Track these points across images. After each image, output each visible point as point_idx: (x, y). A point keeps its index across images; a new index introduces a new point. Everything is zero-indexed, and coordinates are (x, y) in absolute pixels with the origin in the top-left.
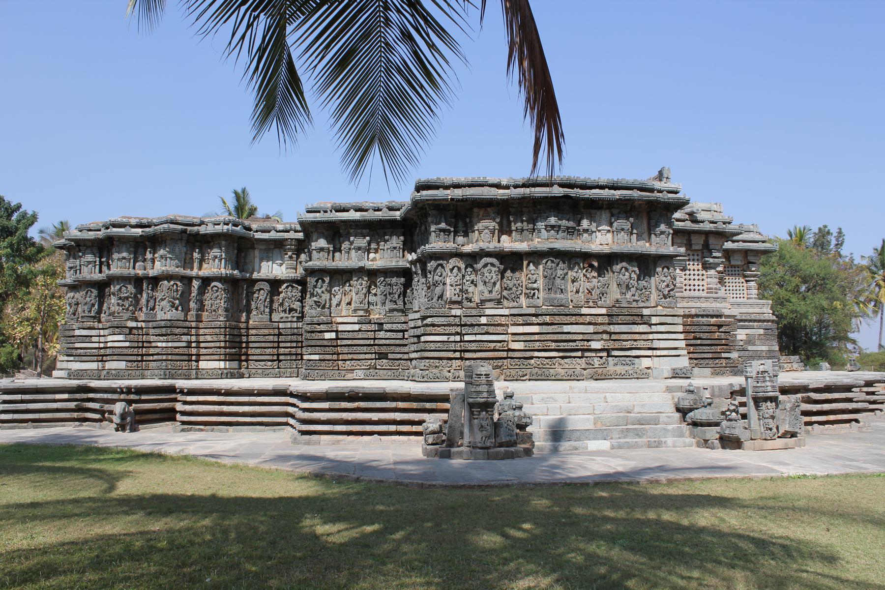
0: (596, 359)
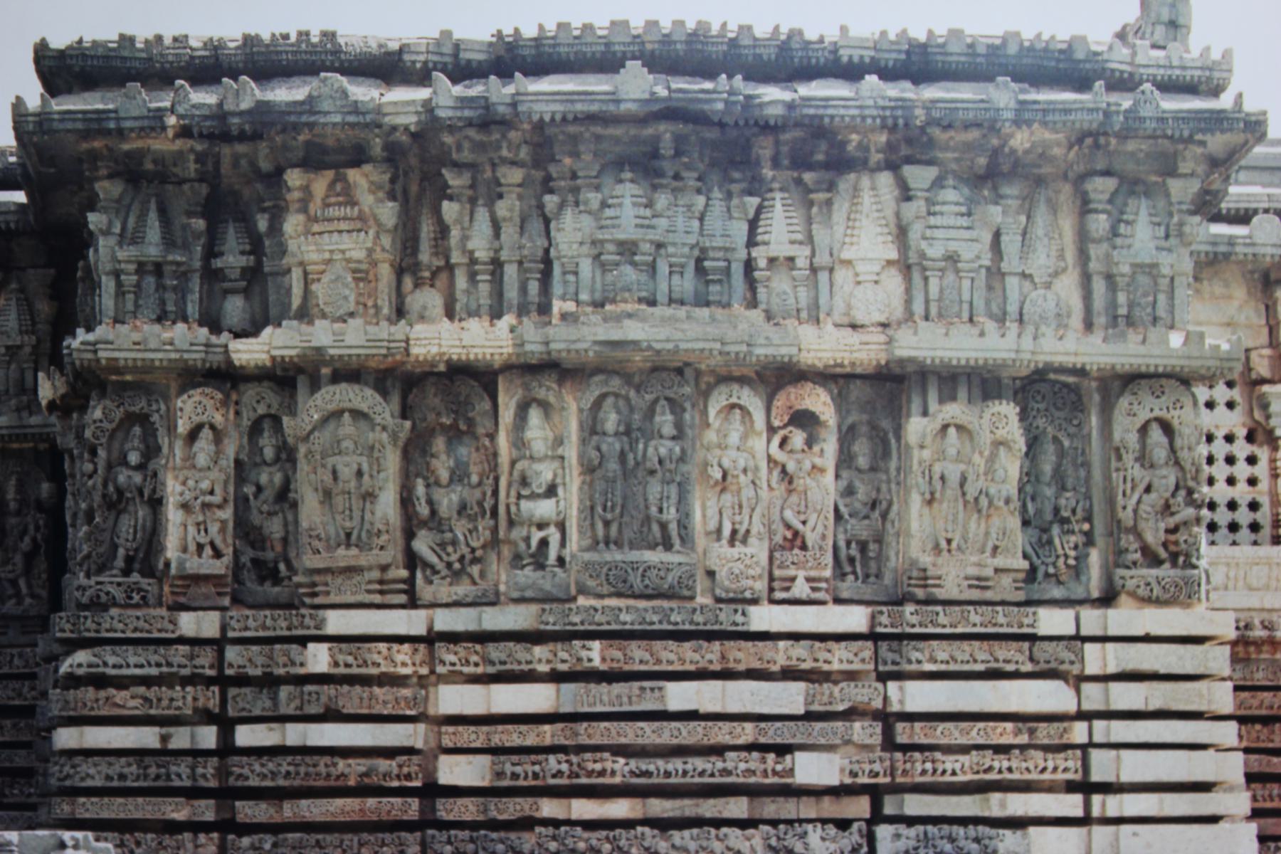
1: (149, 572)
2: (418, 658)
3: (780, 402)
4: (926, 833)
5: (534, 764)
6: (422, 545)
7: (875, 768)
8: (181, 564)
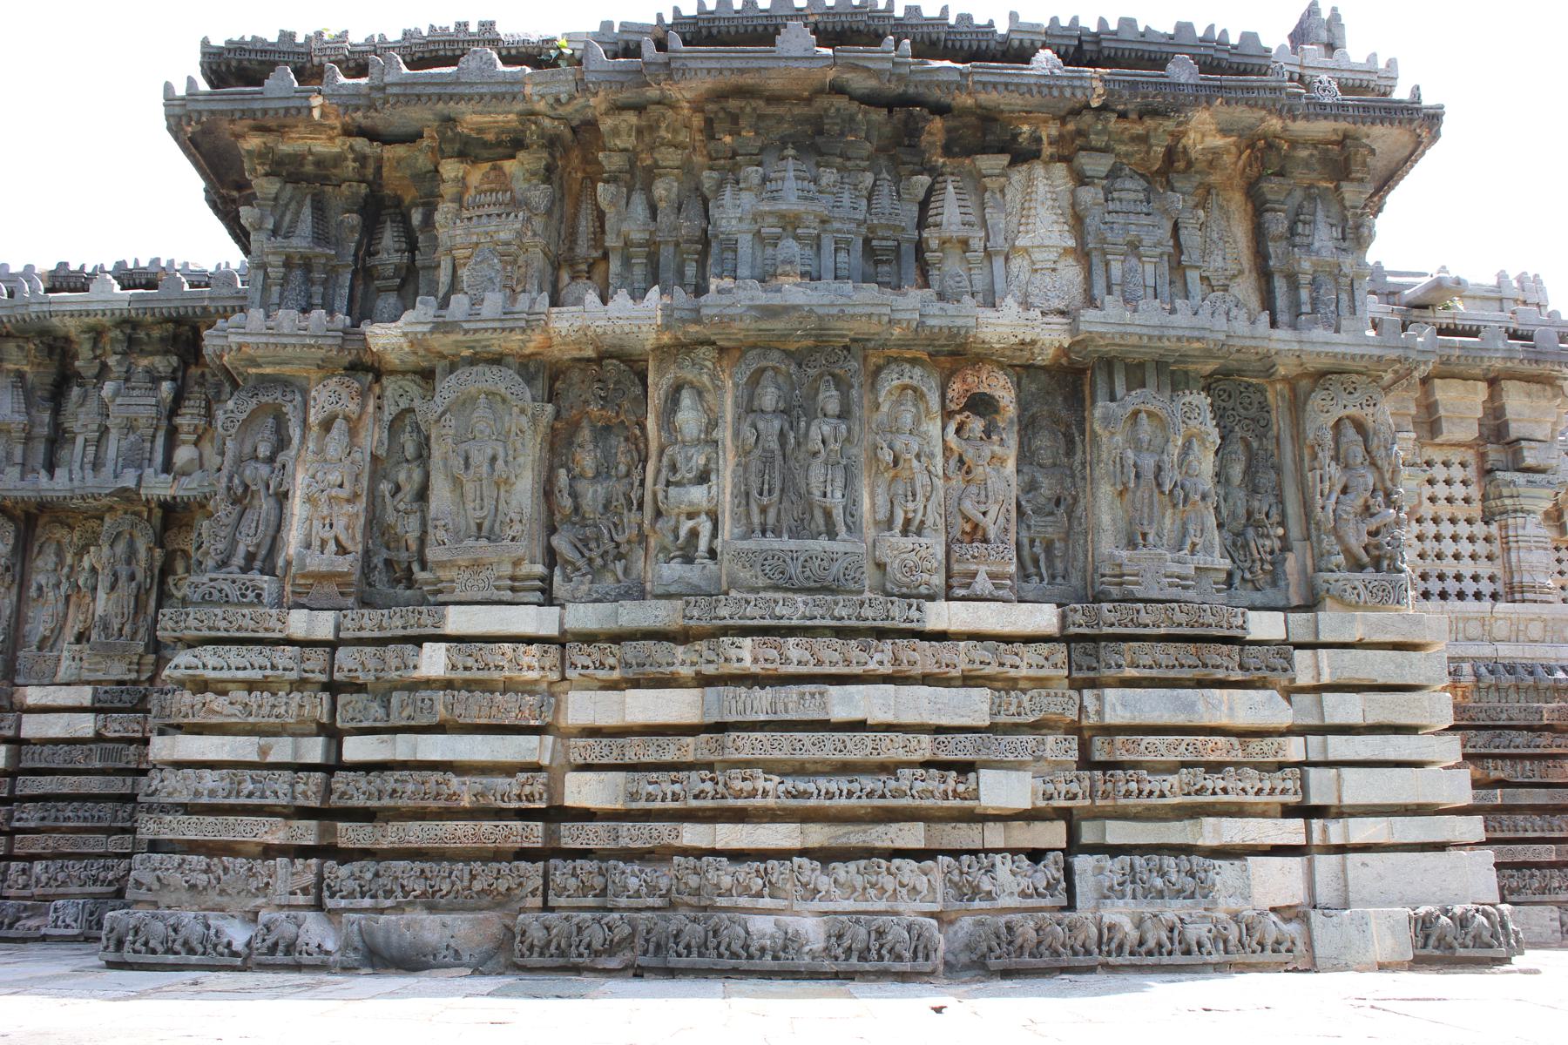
0: (1003, 867)
1: (269, 570)
2: (547, 663)
3: (956, 388)
4: (1132, 866)
5: (673, 782)
6: (560, 542)
7: (1075, 789)
8: (302, 559)
